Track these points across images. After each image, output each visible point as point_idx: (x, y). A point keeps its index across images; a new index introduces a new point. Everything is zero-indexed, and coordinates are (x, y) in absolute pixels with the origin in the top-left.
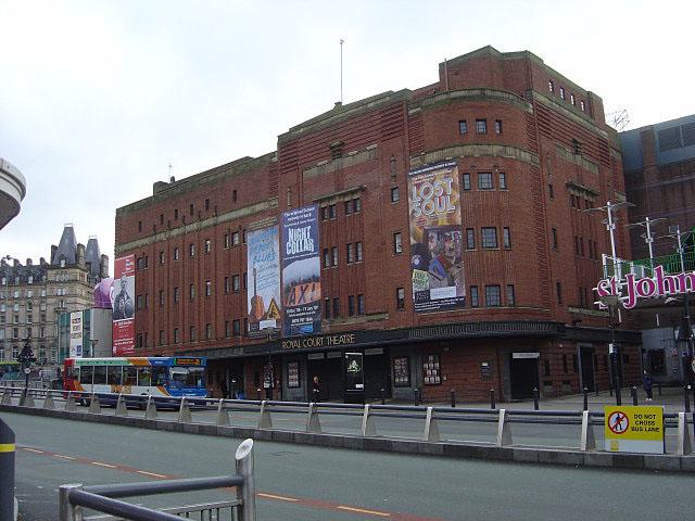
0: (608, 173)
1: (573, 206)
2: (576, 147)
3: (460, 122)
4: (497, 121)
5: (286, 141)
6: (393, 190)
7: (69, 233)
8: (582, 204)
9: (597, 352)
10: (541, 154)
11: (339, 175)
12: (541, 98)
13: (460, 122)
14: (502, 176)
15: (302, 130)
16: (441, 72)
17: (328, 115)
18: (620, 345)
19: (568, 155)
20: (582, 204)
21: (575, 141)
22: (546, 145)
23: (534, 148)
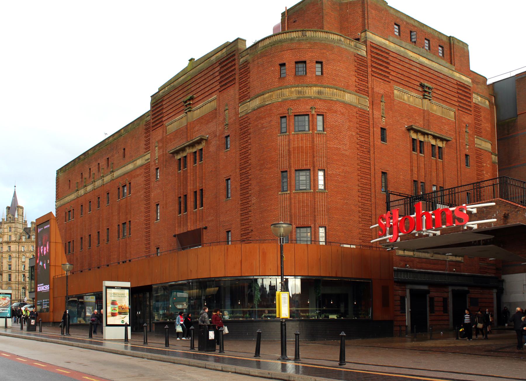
0: (468, 119)
1: (414, 150)
2: (425, 92)
3: (282, 117)
4: (317, 62)
5: (157, 101)
6: (227, 137)
7: (286, 7)
8: (427, 150)
9: (433, 294)
10: (373, 96)
11: (187, 129)
12: (378, 39)
13: (282, 117)
14: (320, 118)
15: (166, 89)
16: (61, 190)
17: (184, 72)
18: (286, 14)
19: (411, 98)
20: (427, 150)
21: (422, 86)
22: (379, 87)
23: (362, 89)
